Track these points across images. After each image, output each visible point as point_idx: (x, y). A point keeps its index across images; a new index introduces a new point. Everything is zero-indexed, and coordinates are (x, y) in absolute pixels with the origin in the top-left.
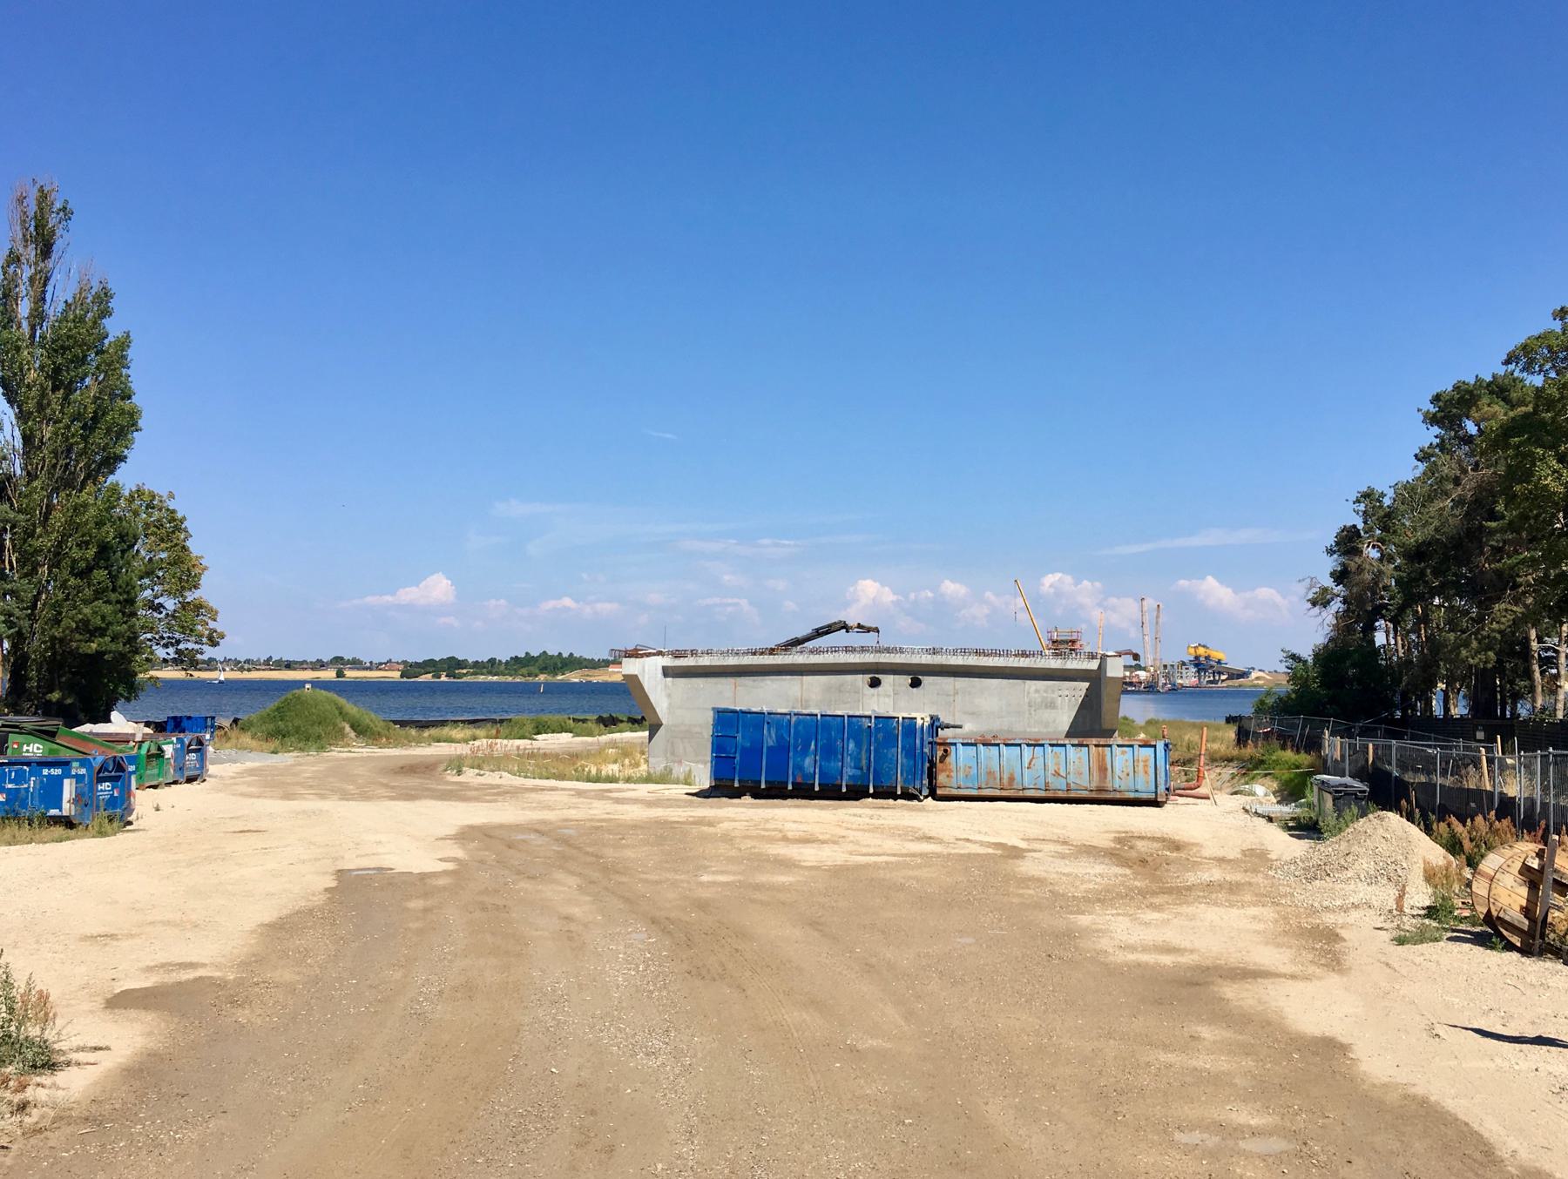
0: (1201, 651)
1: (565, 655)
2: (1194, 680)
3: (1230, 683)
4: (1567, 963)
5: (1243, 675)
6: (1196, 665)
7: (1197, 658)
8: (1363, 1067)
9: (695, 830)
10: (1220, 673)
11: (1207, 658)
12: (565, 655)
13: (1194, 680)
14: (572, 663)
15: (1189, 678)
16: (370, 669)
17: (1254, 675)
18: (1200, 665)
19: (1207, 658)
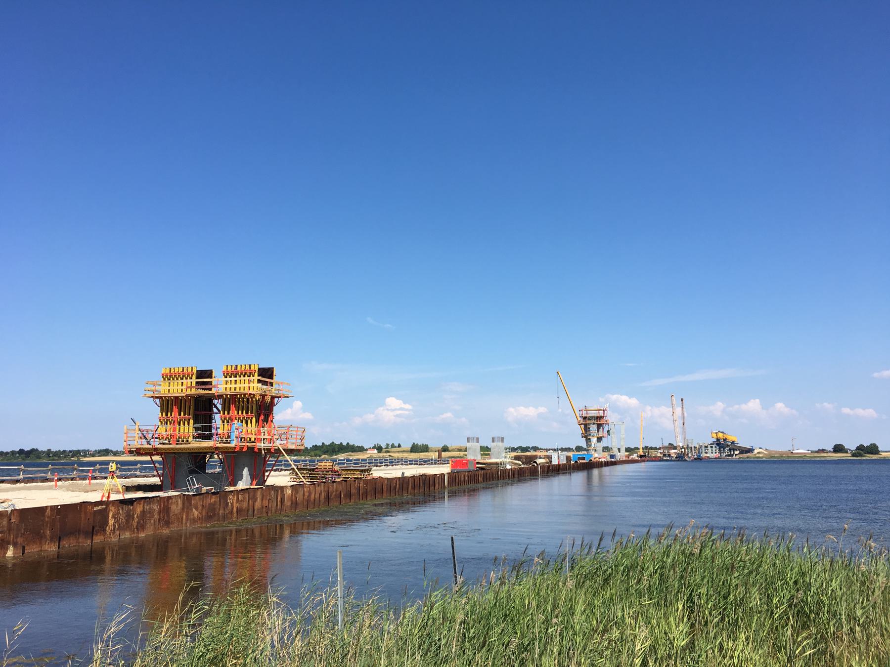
0: (720, 435)
1: (345, 444)
2: (718, 455)
3: (741, 456)
4: (2, 452)
5: (750, 451)
6: (718, 444)
7: (718, 440)
8: (305, 536)
9: (156, 480)
10: (734, 450)
11: (725, 440)
12: (345, 444)
13: (718, 455)
14: (86, 453)
15: (713, 453)
16: (93, 456)
17: (756, 451)
18: (720, 444)
19: (725, 440)
